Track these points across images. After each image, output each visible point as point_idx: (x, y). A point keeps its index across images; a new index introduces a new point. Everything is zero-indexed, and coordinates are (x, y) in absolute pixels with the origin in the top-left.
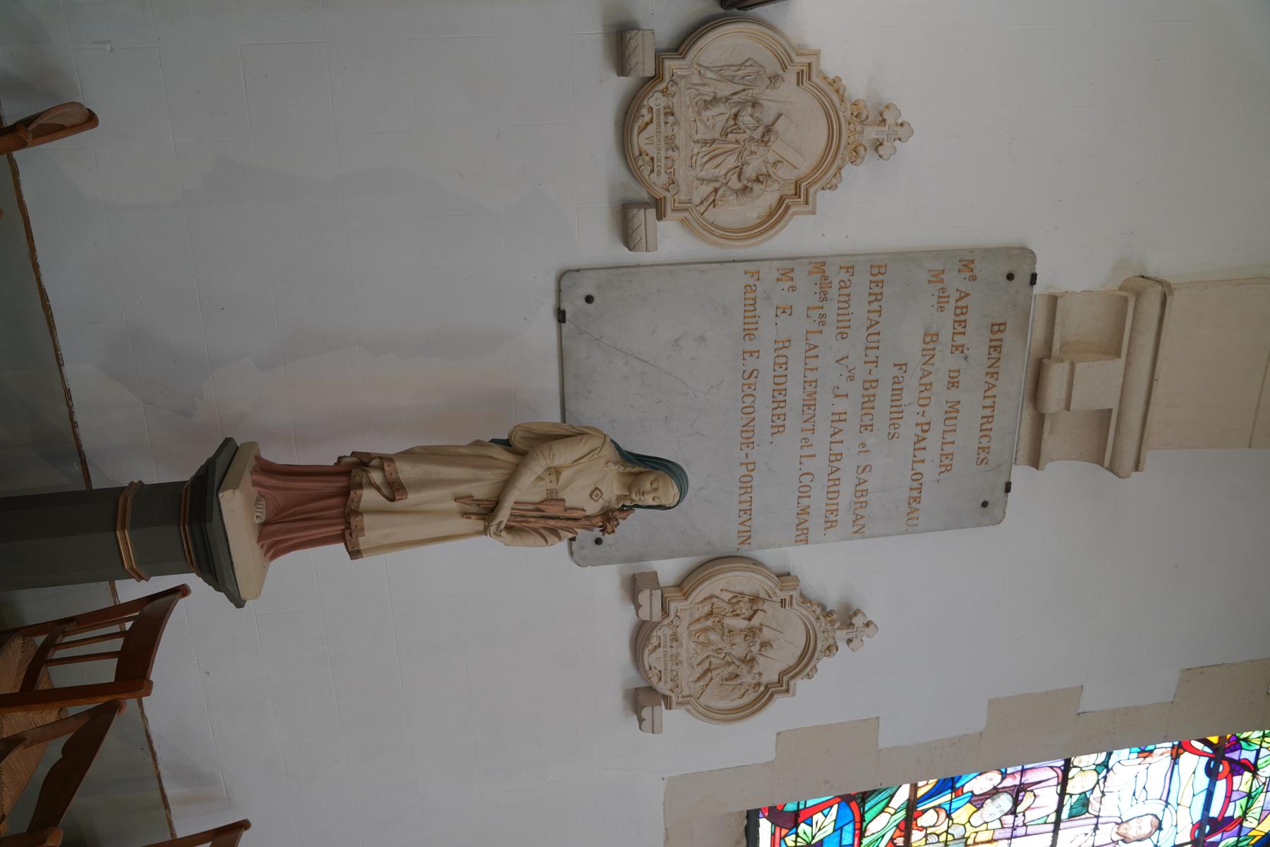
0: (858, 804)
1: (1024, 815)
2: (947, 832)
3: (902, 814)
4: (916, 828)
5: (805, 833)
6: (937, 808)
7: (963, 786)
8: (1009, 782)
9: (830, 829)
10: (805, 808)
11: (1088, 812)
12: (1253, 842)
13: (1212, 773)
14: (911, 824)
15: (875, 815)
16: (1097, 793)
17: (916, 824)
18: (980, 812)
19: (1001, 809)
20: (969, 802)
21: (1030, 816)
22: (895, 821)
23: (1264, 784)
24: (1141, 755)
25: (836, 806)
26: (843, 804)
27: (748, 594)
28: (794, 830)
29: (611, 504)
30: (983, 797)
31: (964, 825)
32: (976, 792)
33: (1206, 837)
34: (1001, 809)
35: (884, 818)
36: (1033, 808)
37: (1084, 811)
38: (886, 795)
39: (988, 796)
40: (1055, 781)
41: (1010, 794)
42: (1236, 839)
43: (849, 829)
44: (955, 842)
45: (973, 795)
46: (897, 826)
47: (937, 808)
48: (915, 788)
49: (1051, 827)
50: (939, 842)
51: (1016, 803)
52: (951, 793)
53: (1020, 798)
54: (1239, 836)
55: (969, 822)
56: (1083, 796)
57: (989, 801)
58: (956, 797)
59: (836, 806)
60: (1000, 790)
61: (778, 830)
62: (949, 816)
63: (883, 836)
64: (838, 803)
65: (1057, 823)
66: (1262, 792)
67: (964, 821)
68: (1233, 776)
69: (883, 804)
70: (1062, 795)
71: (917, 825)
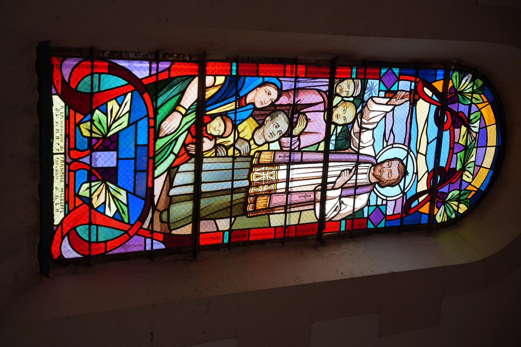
0: (151, 97)
1: (299, 139)
2: (233, 145)
3: (192, 117)
4: (206, 135)
5: (100, 122)
6: (224, 115)
7: (246, 96)
8: (284, 100)
9: (124, 121)
10: (99, 91)
11: (350, 147)
12: (469, 197)
13: (439, 121)
14: (202, 129)
15: (167, 113)
16: (356, 128)
17: (206, 130)
18: (261, 130)
19: (279, 129)
20: (251, 115)
21: (305, 140)
22: (187, 123)
23: (475, 139)
24: (387, 95)
25: (129, 95)
26: (136, 93)
27: (349, 103)
28: (89, 117)
29: (180, 90)
30: (263, 113)
31: (248, 141)
32: (258, 106)
33: (437, 187)
34: (279, 129)
35: (176, 118)
36: (307, 133)
37: (347, 146)
38: (177, 91)
39: (268, 112)
40: (321, 107)
41: (285, 113)
42: (458, 192)
43: (143, 125)
44: (242, 159)
45: (255, 108)
46: (188, 129)
47: (224, 115)
48: (202, 88)
49: (321, 157)
50: (227, 156)
51: (292, 125)
52: (235, 101)
53: (295, 120)
54: (460, 190)
55: (253, 138)
56: (345, 127)
57: (268, 118)
58: (240, 107)
59: (129, 95)
60: (278, 108)
61: (72, 112)
62: (235, 127)
63: (176, 139)
64: (132, 92)
65: (327, 152)
66: (474, 147)
67: (248, 137)
68: (454, 128)
69: (174, 100)
70: (329, 122)
71: (207, 133)
